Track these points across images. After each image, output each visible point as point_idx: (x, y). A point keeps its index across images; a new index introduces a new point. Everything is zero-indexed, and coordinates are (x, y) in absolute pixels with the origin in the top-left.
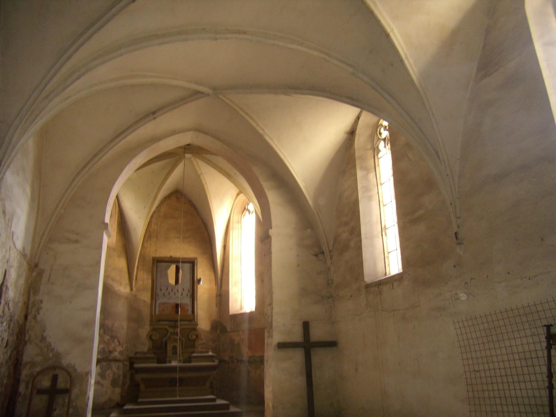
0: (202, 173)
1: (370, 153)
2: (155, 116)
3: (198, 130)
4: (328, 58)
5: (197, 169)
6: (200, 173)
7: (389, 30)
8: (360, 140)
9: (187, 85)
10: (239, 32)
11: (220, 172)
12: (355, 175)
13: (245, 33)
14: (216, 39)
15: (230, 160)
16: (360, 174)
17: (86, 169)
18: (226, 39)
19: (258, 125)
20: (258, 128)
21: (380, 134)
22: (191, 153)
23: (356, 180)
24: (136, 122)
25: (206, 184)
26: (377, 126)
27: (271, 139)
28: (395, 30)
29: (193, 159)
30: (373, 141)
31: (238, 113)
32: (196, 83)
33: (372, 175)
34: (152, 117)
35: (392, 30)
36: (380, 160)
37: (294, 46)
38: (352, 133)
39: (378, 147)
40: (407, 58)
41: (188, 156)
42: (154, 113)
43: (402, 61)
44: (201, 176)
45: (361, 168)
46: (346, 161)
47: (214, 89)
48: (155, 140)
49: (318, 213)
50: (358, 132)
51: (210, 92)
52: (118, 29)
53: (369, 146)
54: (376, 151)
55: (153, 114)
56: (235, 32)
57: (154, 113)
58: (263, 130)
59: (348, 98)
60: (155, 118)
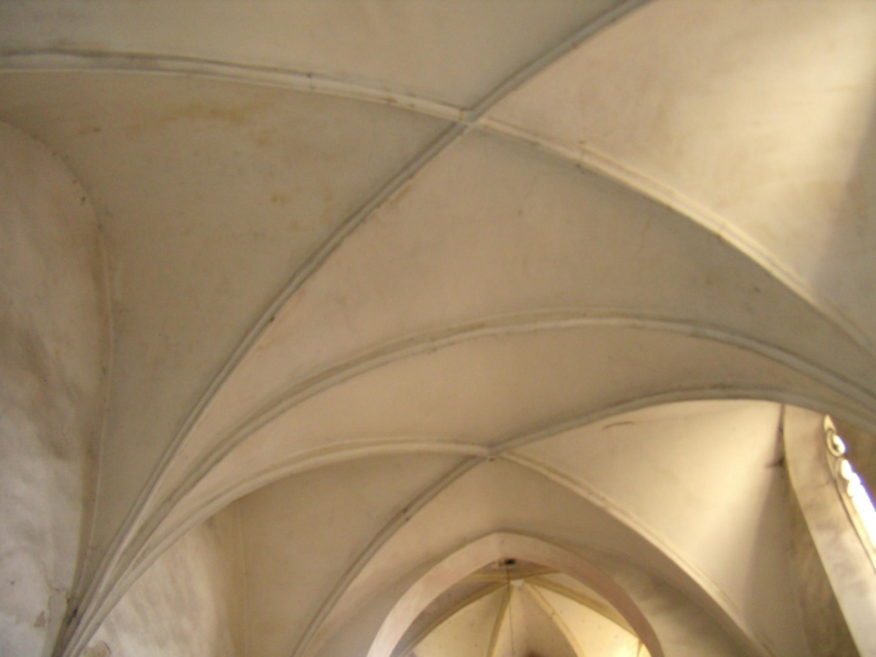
0: (554, 613)
1: (829, 491)
2: (408, 514)
3: (505, 529)
4: (638, 322)
5: (543, 604)
6: (550, 612)
7: (714, 228)
8: (800, 473)
9: (436, 447)
10: (472, 328)
11: (581, 603)
12: (811, 544)
13: (481, 326)
14: (435, 349)
15: (574, 572)
16: (820, 539)
17: (312, 630)
18: (452, 344)
19: (590, 493)
20: (592, 499)
21: (835, 447)
22: (520, 577)
23: (816, 555)
24: (382, 532)
25: (568, 630)
26: (822, 435)
27: (625, 513)
28: (731, 226)
29: (528, 586)
30: (826, 466)
31: (546, 478)
32: (456, 442)
33: (848, 537)
34: (403, 518)
35: (723, 227)
36: (854, 500)
37: (571, 322)
38: (779, 462)
39: (840, 475)
40: (774, 264)
41: (517, 583)
42: (405, 510)
43: (767, 274)
44: (555, 618)
45: (821, 527)
46: (785, 521)
47: (491, 445)
48: (431, 561)
49: (765, 646)
50: (789, 457)
51: (485, 451)
52: (260, 373)
53: (822, 478)
54: (839, 483)
55: (402, 514)
56: (464, 330)
57: (405, 510)
58: (603, 499)
59: (715, 387)
60: (408, 519)
